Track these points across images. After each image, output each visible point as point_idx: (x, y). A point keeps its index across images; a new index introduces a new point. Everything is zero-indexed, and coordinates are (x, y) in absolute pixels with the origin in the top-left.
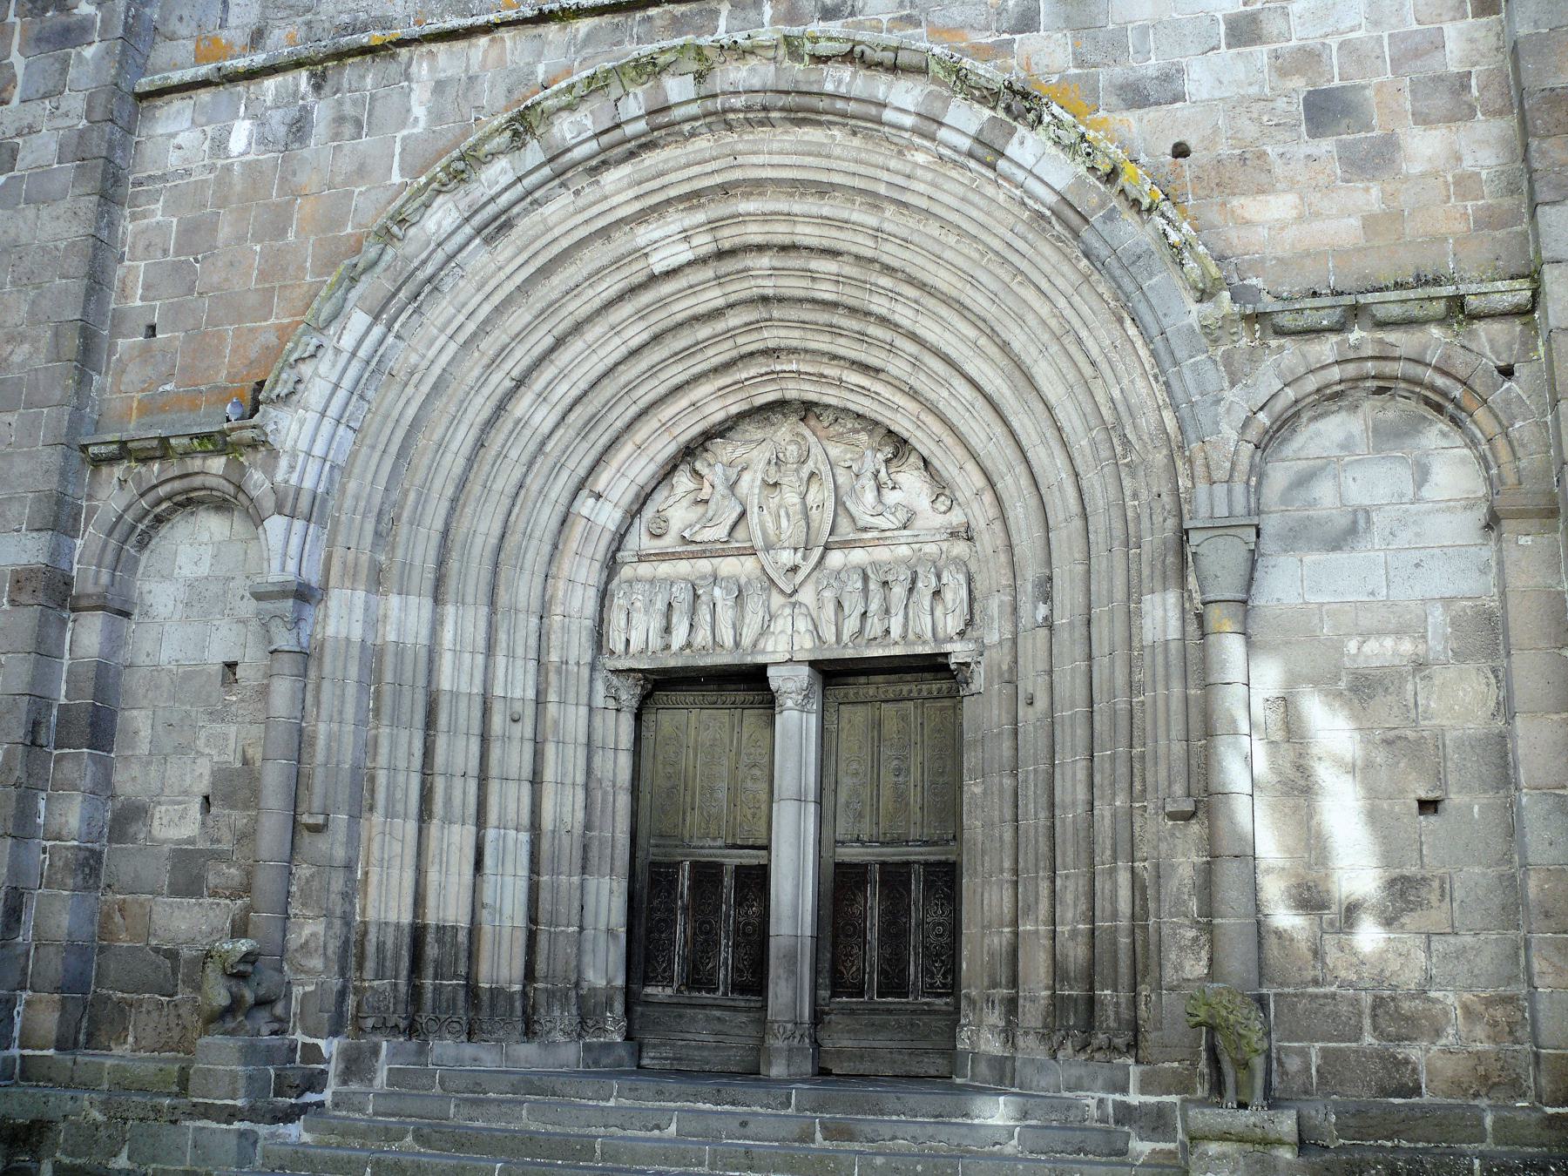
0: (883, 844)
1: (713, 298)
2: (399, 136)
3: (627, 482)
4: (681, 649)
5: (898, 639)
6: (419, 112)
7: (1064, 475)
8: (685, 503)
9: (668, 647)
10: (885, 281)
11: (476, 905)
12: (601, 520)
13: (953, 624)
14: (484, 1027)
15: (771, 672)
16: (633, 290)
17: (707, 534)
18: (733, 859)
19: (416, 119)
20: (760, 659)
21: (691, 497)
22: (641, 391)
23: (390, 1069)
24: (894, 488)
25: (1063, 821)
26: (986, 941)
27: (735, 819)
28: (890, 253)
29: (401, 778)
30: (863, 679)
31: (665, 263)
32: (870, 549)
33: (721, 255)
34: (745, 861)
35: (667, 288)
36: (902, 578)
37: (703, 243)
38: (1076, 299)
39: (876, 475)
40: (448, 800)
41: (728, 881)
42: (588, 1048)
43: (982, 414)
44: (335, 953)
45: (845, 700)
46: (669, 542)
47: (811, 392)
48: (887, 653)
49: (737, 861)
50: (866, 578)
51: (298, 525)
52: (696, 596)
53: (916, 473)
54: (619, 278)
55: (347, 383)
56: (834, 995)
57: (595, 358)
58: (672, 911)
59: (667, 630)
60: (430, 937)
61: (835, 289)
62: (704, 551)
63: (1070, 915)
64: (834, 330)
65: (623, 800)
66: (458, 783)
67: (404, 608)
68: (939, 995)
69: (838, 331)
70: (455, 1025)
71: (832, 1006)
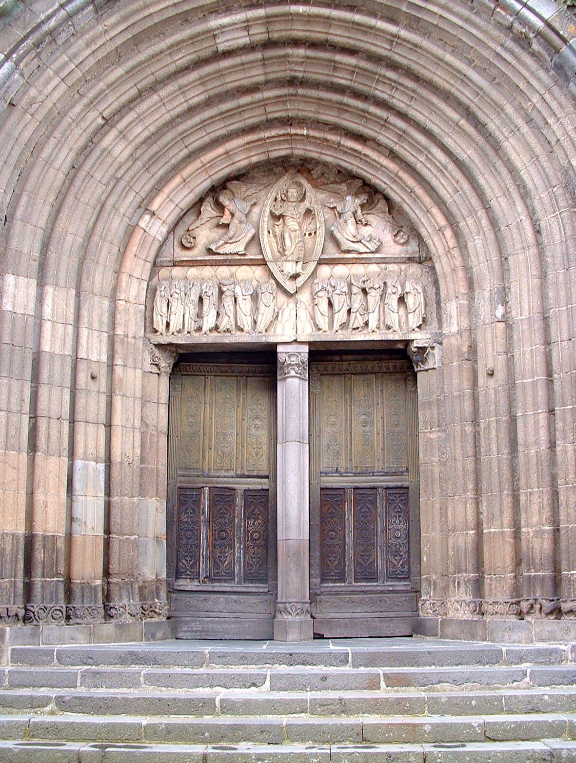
0: (355, 475)
1: (257, 75)
3: (173, 206)
4: (211, 330)
5: (374, 328)
7: (523, 217)
8: (208, 225)
9: (199, 329)
10: (391, 74)
11: (71, 519)
12: (153, 232)
13: (414, 320)
14: (78, 613)
15: (280, 349)
16: (206, 61)
17: (229, 249)
18: (242, 485)
20: (272, 340)
21: (214, 221)
22: (192, 139)
23: (13, 650)
24: (366, 225)
25: (527, 456)
26: (451, 541)
27: (243, 455)
28: (400, 56)
29: (14, 418)
30: (337, 358)
31: (227, 44)
33: (269, 44)
34: (251, 487)
35: (225, 63)
36: (377, 286)
37: (259, 33)
38: (547, 97)
39: (354, 214)
41: (239, 501)
43: (453, 173)
45: (325, 372)
46: (197, 253)
47: (313, 152)
48: (367, 338)
49: (246, 487)
50: (350, 285)
52: (221, 293)
53: (381, 215)
54: (191, 51)
56: (323, 580)
57: (164, 110)
58: (197, 523)
59: (200, 316)
60: (38, 545)
61: (350, 77)
62: (225, 260)
63: (535, 519)
64: (342, 107)
65: (163, 440)
66: (54, 423)
67: (16, 286)
68: (400, 579)
69: (345, 108)
70: (58, 612)
71: (322, 590)
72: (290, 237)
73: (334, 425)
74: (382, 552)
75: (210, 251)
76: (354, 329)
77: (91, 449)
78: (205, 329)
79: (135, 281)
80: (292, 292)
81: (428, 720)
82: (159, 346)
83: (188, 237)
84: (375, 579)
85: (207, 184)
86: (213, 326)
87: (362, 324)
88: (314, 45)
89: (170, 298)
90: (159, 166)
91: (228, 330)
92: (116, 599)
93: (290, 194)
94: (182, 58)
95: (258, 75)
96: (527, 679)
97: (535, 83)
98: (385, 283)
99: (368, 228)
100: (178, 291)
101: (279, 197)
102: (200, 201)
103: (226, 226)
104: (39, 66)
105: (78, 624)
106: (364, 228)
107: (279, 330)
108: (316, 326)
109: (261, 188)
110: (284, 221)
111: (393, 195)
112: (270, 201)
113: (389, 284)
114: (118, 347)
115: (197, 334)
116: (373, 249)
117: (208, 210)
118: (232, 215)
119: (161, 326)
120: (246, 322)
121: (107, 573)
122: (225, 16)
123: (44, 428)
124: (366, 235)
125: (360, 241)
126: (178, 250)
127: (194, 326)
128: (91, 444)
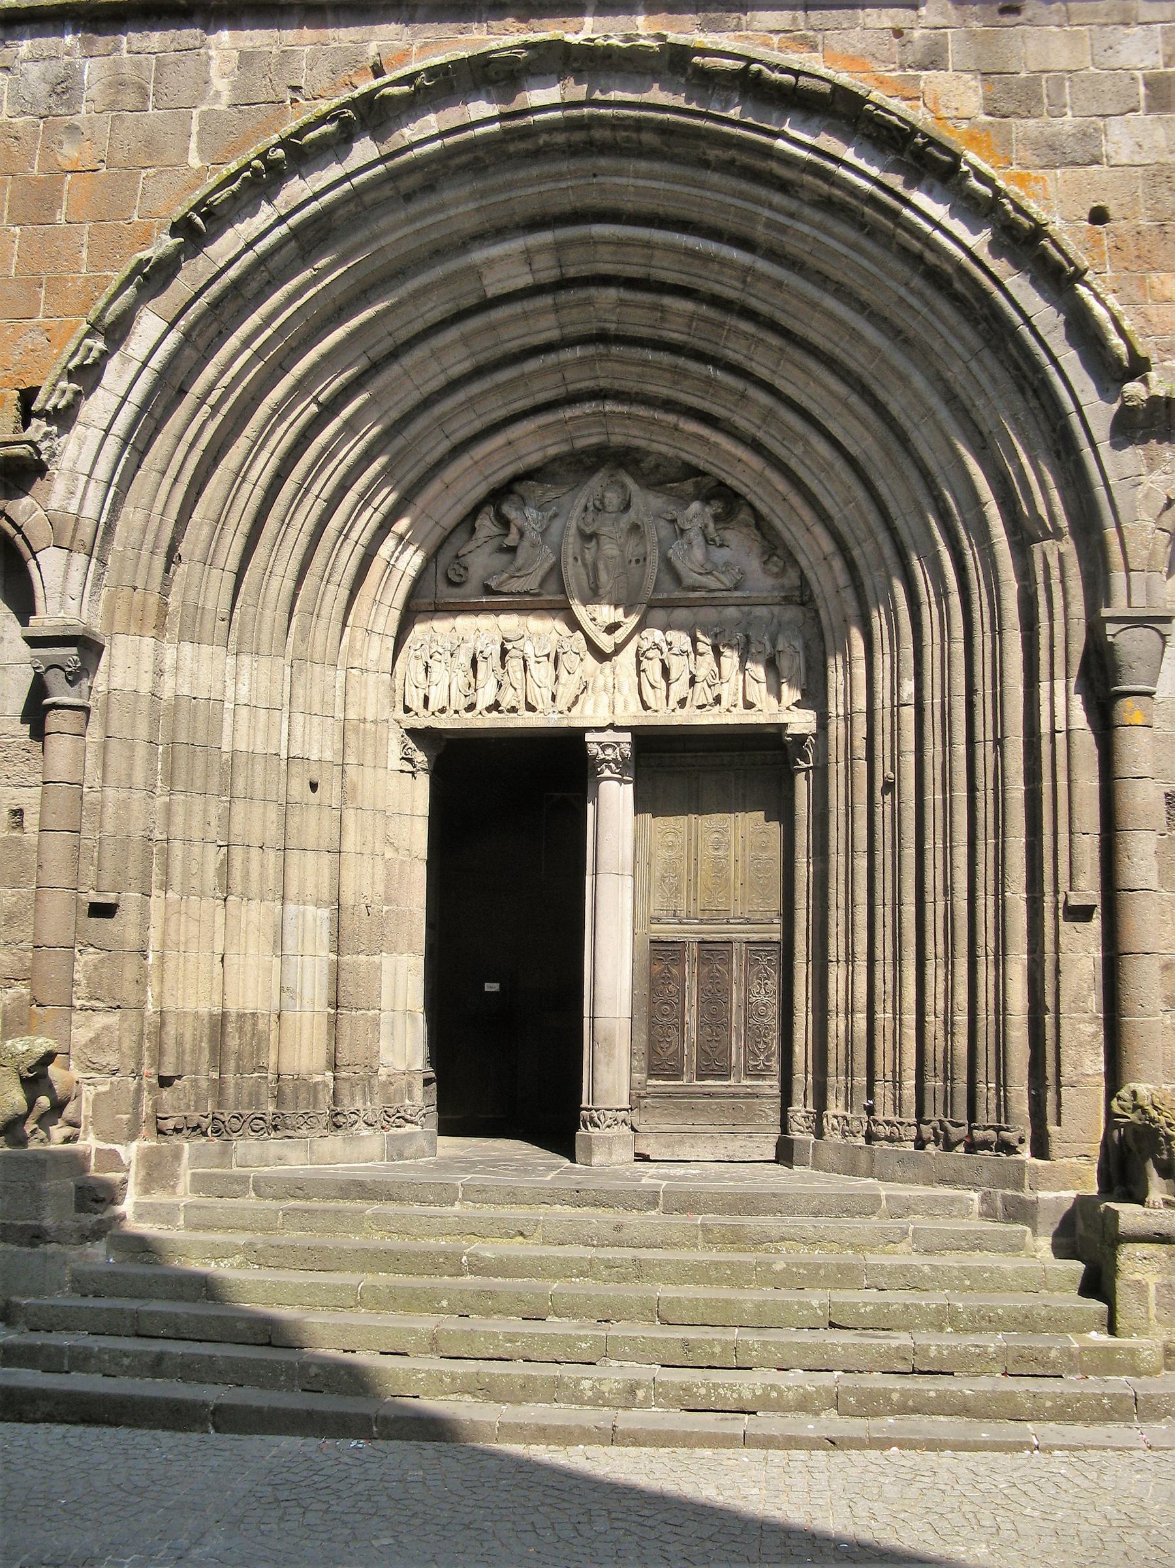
1: (546, 329)
2: (195, 113)
3: (431, 523)
6: (221, 85)
15: (588, 737)
17: (516, 585)
19: (218, 94)
20: (578, 724)
21: (495, 543)
23: (193, 1174)
24: (721, 546)
32: (695, 609)
40: (246, 875)
42: (393, 1138)
44: (131, 1048)
48: (718, 721)
51: (80, 559)
52: (504, 652)
53: (745, 530)
55: (136, 396)
59: (472, 687)
72: (606, 567)
73: (671, 847)
74: (738, 1036)
75: (488, 590)
76: (699, 707)
77: (310, 889)
78: (479, 707)
79: (376, 638)
80: (608, 651)
81: (750, 1296)
82: (412, 733)
83: (456, 567)
84: (726, 1077)
85: (481, 491)
86: (492, 702)
87: (711, 701)
88: (631, 283)
89: (430, 661)
90: (406, 468)
91: (513, 710)
92: (346, 1102)
93: (606, 501)
94: (432, 309)
95: (438, 443)
96: (909, 1239)
97: (956, 345)
98: (747, 637)
99: (725, 551)
100: (441, 651)
101: (590, 505)
102: (475, 511)
103: (512, 550)
104: (220, 332)
105: (290, 1137)
106: (717, 550)
107: (588, 711)
108: (643, 702)
109: (564, 490)
110: (598, 543)
111: (758, 504)
112: (577, 512)
113: (753, 639)
114: (351, 738)
115: (469, 715)
116: (729, 585)
117: (486, 525)
118: (522, 534)
119: (416, 703)
120: (540, 697)
121: (334, 1066)
122: (495, 244)
123: (240, 861)
124: (720, 562)
125: (710, 573)
126: (442, 587)
127: (465, 703)
128: (310, 882)
